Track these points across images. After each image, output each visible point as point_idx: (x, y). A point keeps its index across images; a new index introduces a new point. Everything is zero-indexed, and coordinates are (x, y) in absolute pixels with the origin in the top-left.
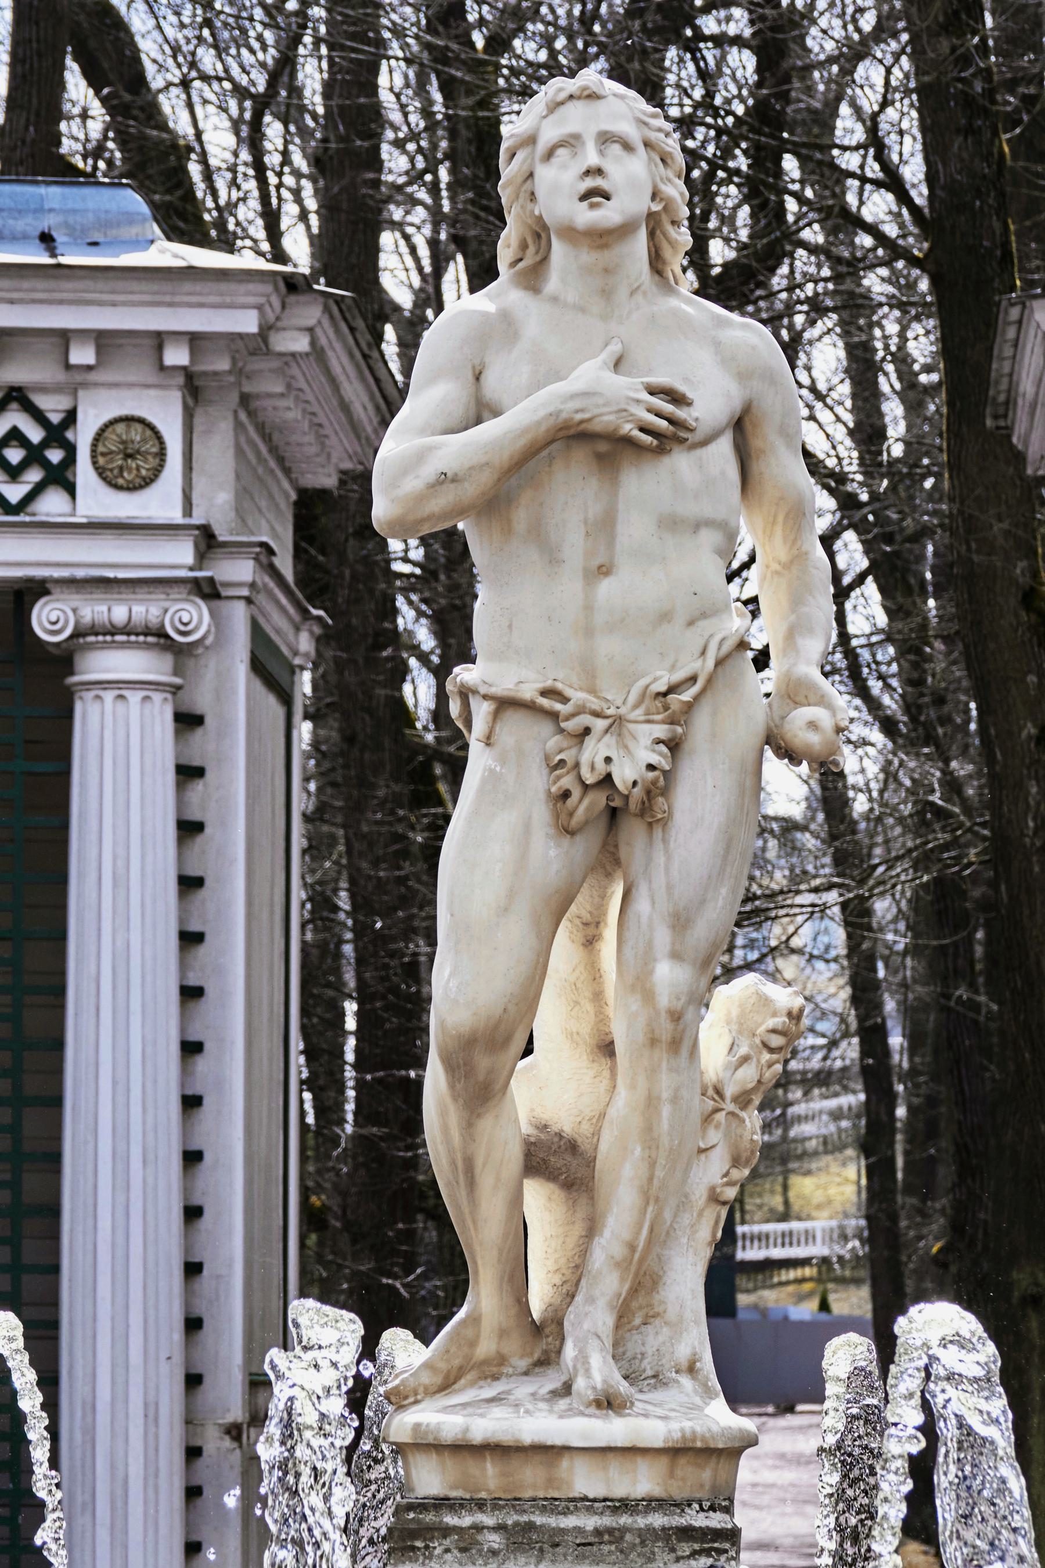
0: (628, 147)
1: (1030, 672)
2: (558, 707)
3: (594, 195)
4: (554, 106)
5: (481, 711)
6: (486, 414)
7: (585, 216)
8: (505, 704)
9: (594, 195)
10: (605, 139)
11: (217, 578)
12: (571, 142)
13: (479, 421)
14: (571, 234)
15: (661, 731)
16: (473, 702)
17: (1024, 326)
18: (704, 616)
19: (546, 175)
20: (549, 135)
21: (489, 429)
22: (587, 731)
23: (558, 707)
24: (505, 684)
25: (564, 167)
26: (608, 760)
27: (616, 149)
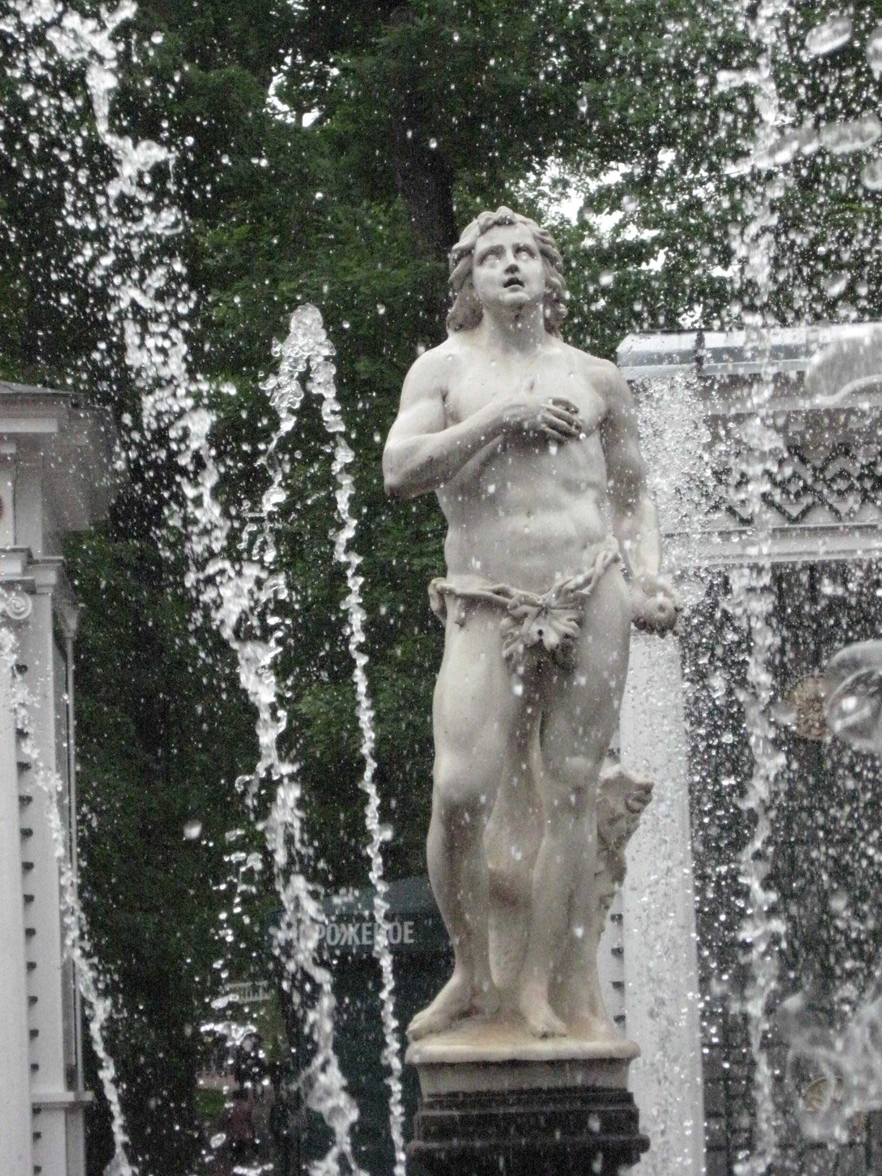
0: (531, 254)
1: (271, 167)
2: (506, 600)
3: (513, 283)
4: (485, 230)
5: (454, 611)
6: (450, 422)
7: (508, 296)
8: (471, 602)
9: (513, 283)
10: (518, 250)
11: (37, 582)
12: (497, 251)
13: (445, 426)
14: (497, 304)
15: (573, 615)
16: (449, 602)
17: (79, 1060)
18: (592, 542)
19: (482, 273)
20: (483, 245)
21: (455, 431)
22: (526, 615)
23: (506, 600)
24: (476, 586)
25: (493, 266)
26: (540, 633)
27: (524, 256)
